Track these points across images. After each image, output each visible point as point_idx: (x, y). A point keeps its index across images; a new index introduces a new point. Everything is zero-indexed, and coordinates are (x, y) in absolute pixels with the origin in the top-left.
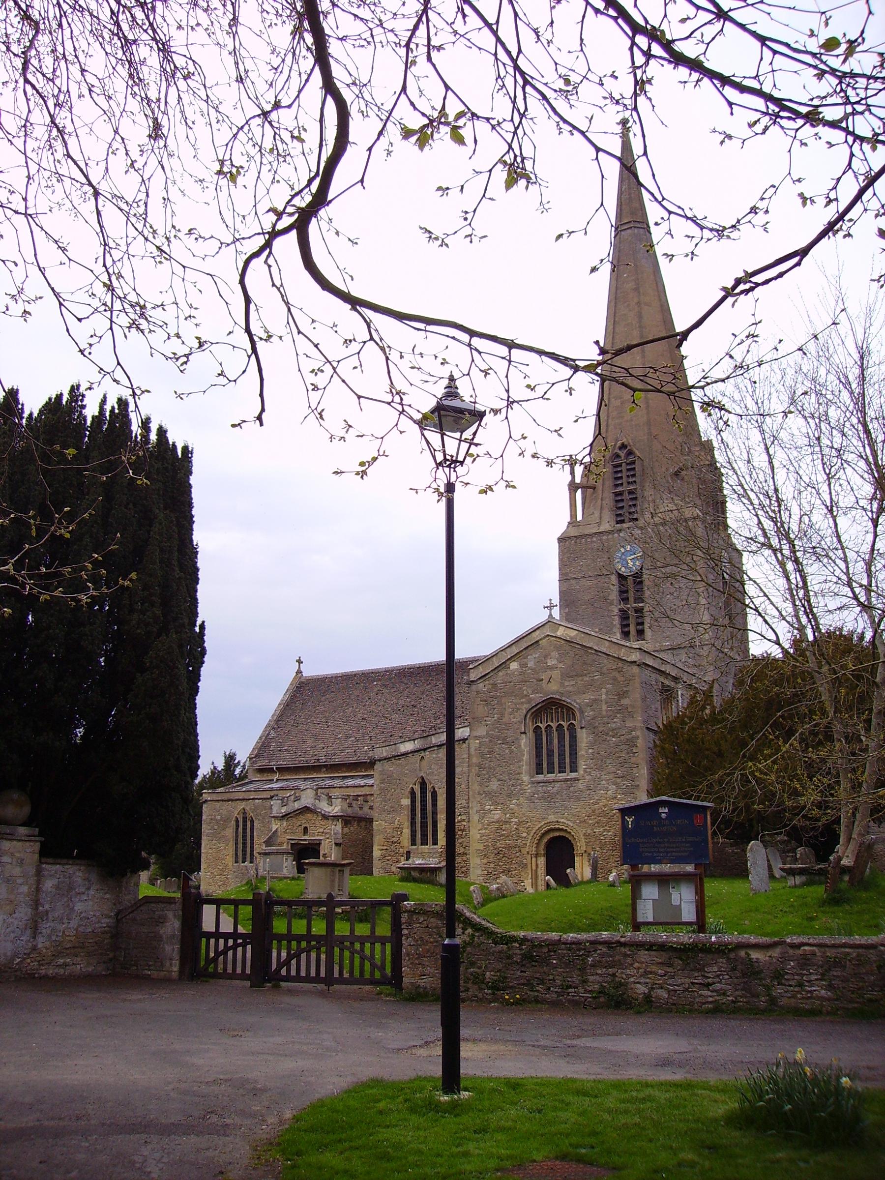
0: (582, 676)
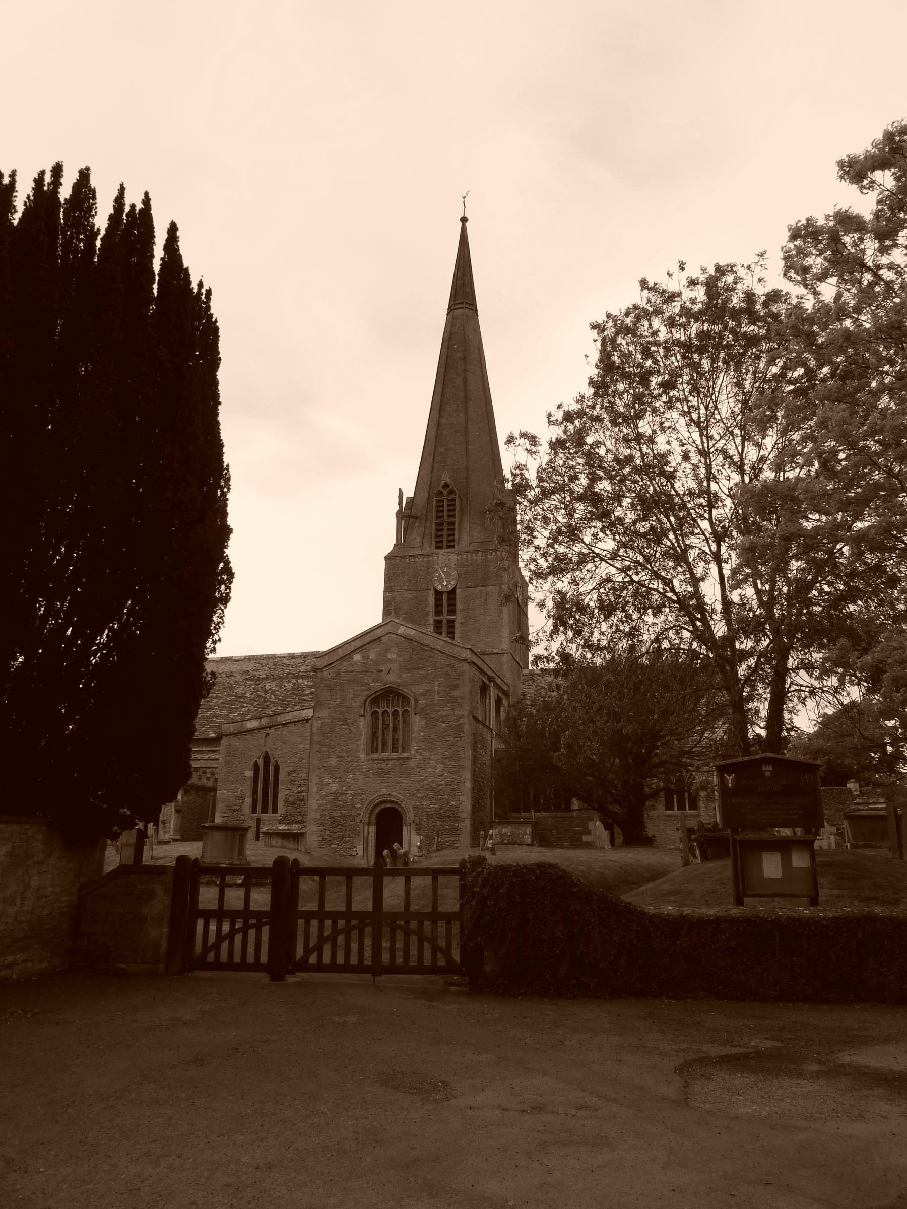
0: (417, 669)
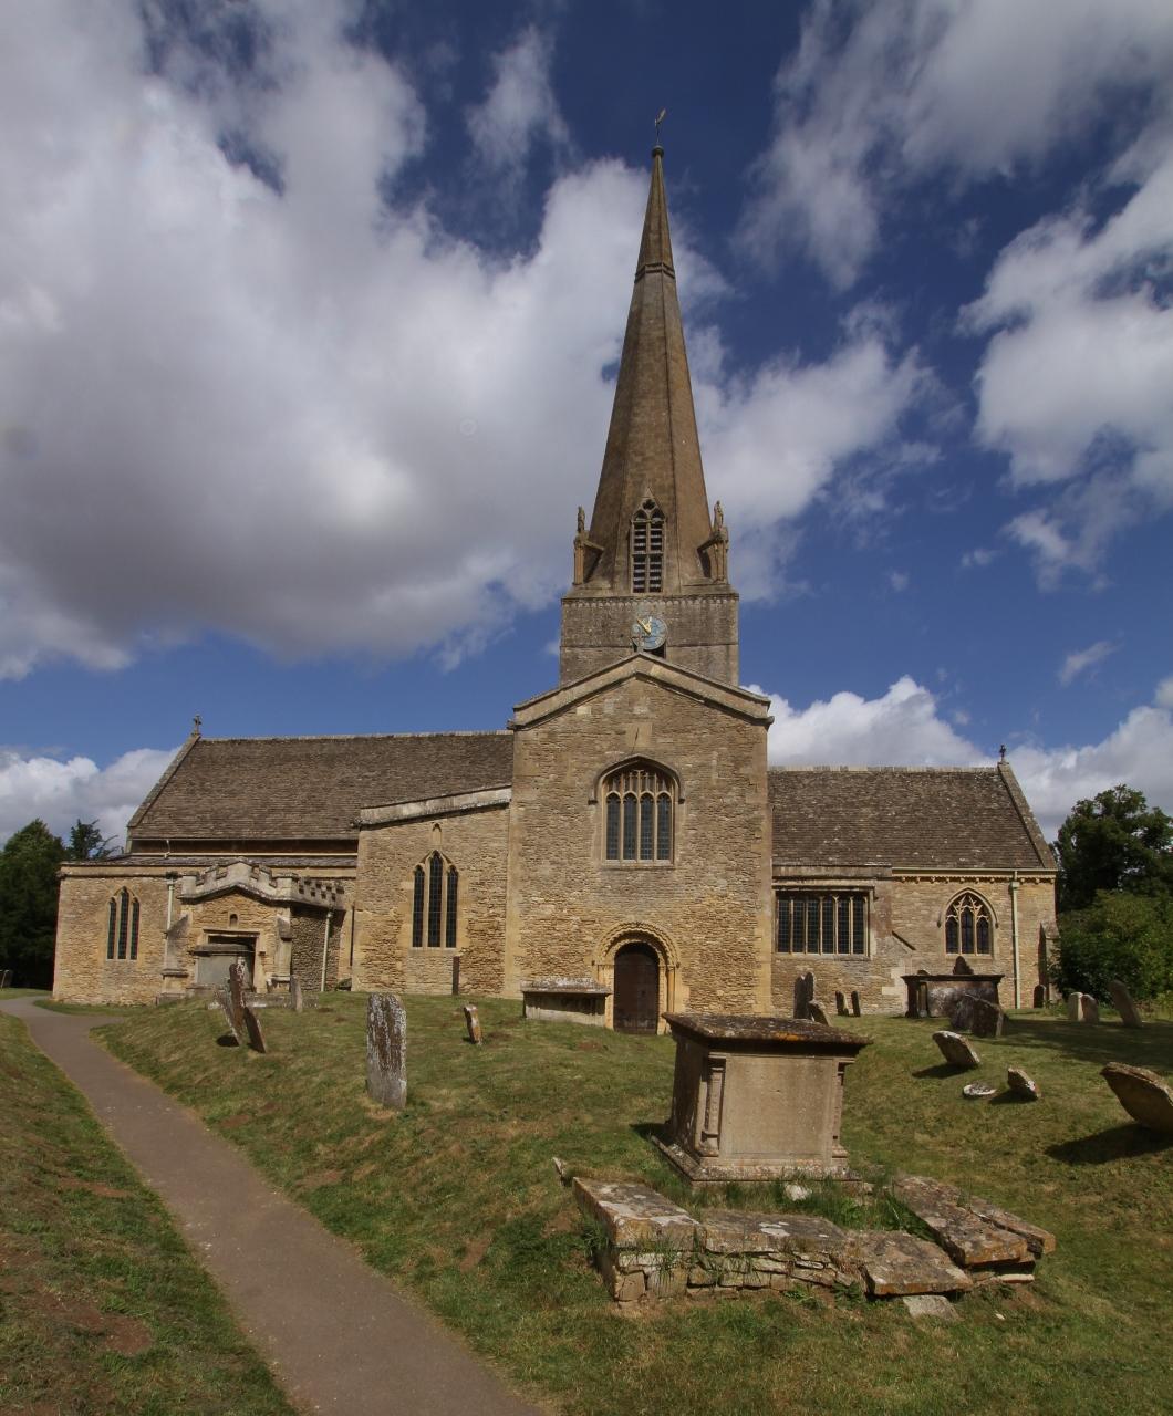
0: (683, 731)
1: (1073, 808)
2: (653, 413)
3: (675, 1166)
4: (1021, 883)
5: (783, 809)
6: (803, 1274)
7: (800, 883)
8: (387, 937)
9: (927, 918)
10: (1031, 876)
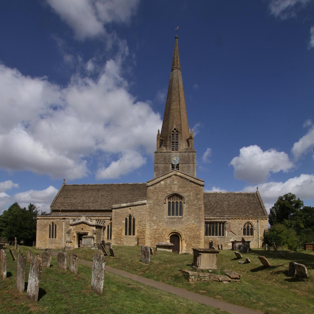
1: (278, 199)
2: (176, 106)
3: (194, 268)
4: (260, 220)
5: (207, 202)
6: (211, 279)
7: (210, 220)
8: (119, 233)
9: (239, 228)
10: (262, 218)
